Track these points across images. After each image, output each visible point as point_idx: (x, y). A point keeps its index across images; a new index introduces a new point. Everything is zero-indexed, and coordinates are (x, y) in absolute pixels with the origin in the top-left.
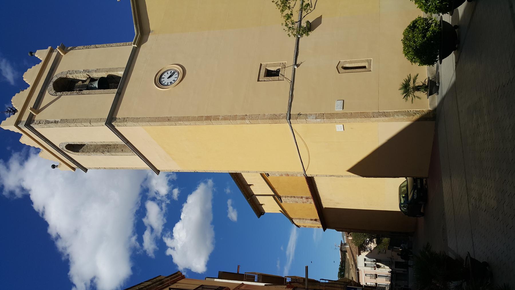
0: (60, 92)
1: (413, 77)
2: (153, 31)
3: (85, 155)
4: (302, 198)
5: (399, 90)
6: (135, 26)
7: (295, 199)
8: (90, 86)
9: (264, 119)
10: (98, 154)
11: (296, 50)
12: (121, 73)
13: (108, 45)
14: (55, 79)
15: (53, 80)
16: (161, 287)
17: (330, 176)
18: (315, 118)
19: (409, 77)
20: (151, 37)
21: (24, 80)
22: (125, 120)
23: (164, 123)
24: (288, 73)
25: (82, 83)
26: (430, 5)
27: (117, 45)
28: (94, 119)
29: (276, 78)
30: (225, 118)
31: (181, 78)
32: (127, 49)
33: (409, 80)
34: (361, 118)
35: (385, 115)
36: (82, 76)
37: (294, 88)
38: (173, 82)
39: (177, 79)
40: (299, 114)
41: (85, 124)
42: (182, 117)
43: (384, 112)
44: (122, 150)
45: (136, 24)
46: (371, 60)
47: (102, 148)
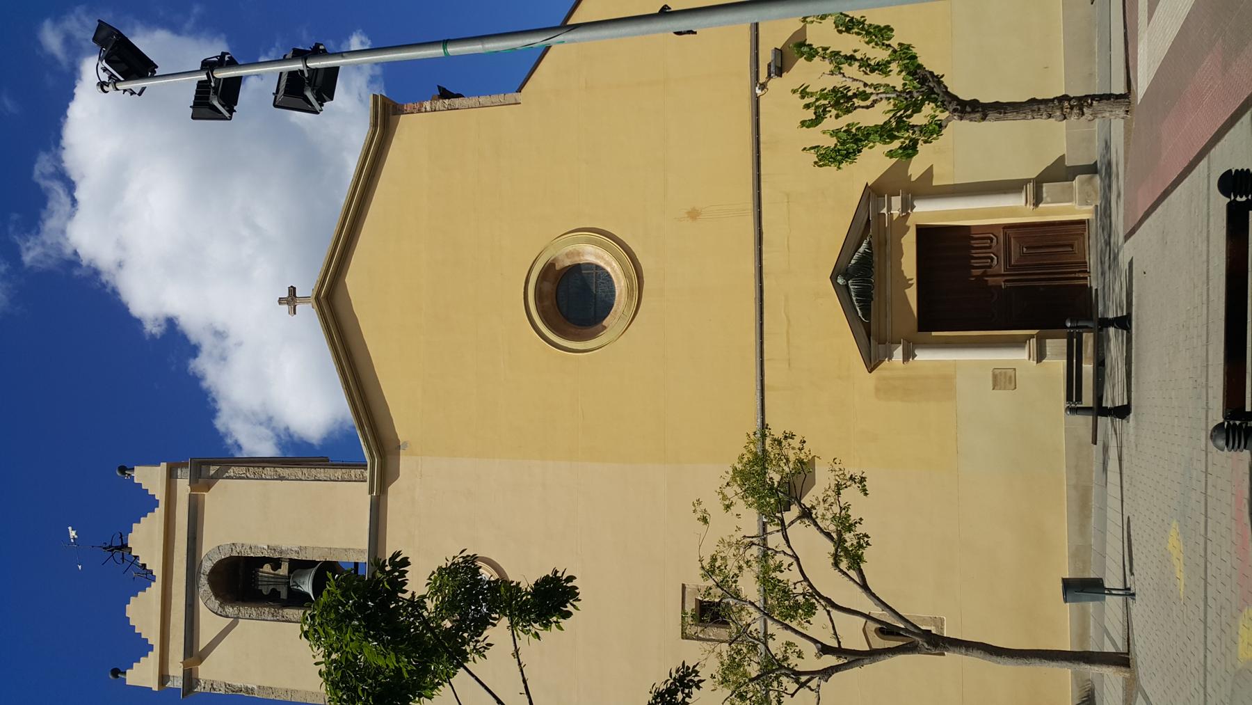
2: (405, 443)
8: (296, 587)
14: (207, 566)
20: (406, 462)
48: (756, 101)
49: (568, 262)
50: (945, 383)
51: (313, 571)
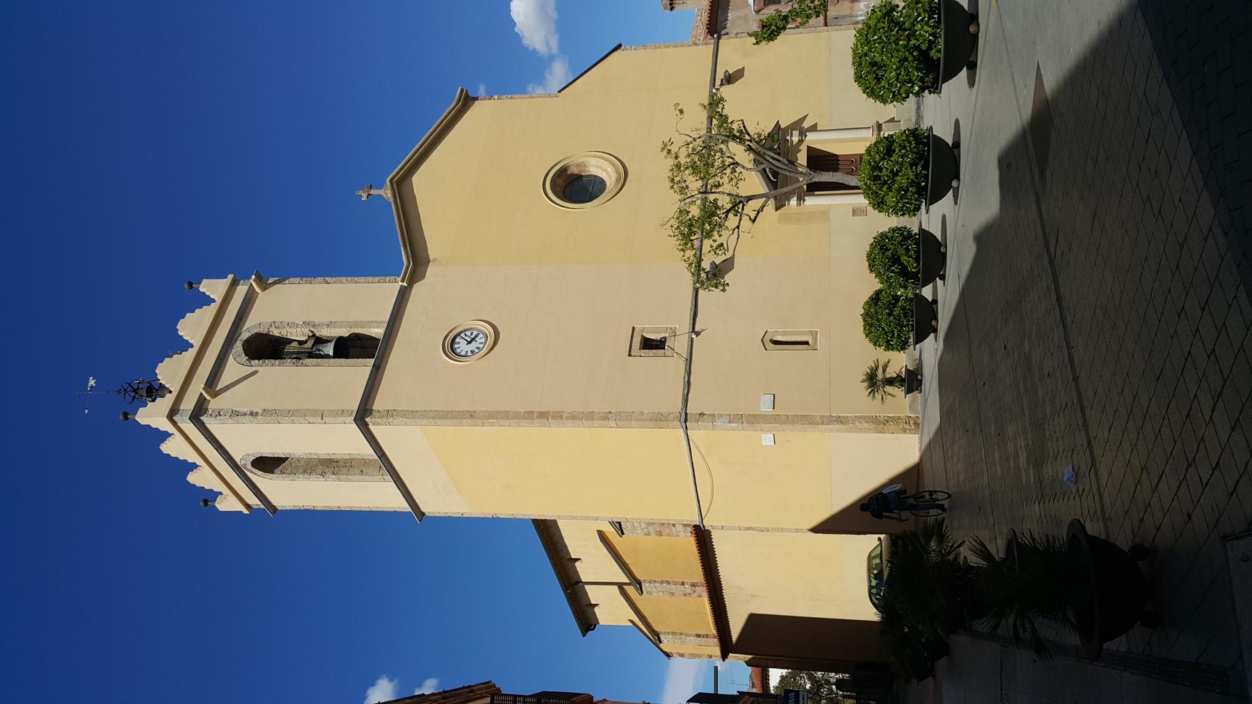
0: (259, 359)
2: (435, 260)
3: (285, 479)
4: (683, 584)
5: (862, 382)
6: (402, 249)
7: (669, 586)
8: (318, 352)
9: (640, 420)
10: (313, 477)
11: (693, 307)
12: (378, 332)
13: (349, 279)
14: (245, 335)
15: (241, 336)
16: (472, 696)
17: (746, 529)
18: (727, 421)
20: (430, 270)
21: (180, 333)
22: (389, 414)
23: (463, 421)
24: (680, 344)
25: (298, 346)
26: (893, 282)
27: (367, 280)
28: (329, 410)
29: (660, 352)
30: (574, 417)
31: (491, 344)
32: (389, 290)
33: (877, 368)
34: (803, 424)
35: (840, 420)
36: (299, 333)
37: (692, 370)
38: (477, 351)
39: (484, 346)
40: (702, 414)
42: (496, 411)
43: (839, 417)
45: (405, 246)
46: (816, 332)
47: (321, 467)
49: (575, 170)
50: (823, 214)
51: (333, 343)
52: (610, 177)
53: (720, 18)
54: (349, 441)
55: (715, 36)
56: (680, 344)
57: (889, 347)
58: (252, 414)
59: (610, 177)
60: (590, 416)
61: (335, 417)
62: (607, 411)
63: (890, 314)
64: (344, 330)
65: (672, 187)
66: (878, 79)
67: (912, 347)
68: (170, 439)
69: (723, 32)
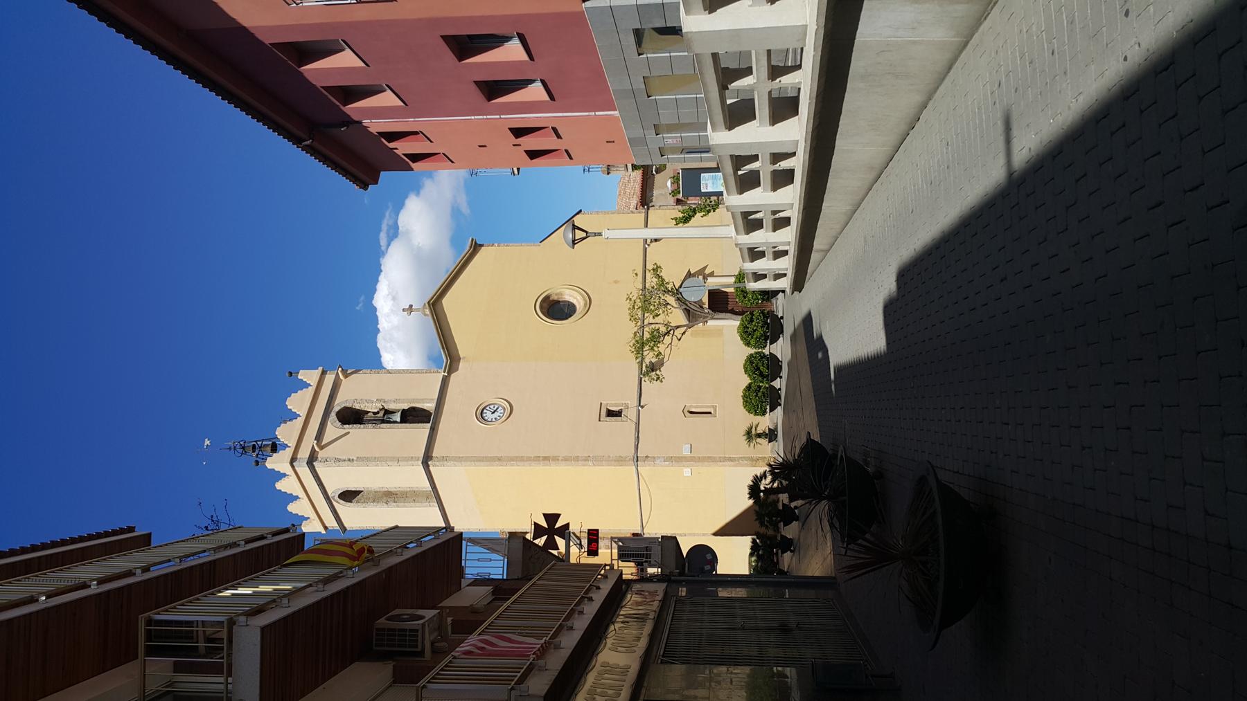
1: (754, 425)
2: (464, 358)
10: (379, 505)
12: (430, 406)
14: (337, 409)
19: (402, 148)
20: (462, 365)
22: (444, 459)
24: (632, 413)
30: (566, 459)
31: (509, 413)
33: (751, 428)
35: (731, 459)
40: (647, 457)
41: (390, 463)
44: (414, 500)
48: (645, 250)
49: (555, 298)
52: (579, 303)
53: (648, 194)
54: (414, 478)
55: (646, 207)
56: (632, 413)
57: (756, 414)
58: (349, 460)
59: (579, 303)
60: (577, 459)
61: (407, 461)
62: (587, 455)
63: (756, 396)
64: (406, 405)
65: (630, 319)
66: (745, 297)
67: (768, 414)
68: (286, 478)
69: (650, 205)
